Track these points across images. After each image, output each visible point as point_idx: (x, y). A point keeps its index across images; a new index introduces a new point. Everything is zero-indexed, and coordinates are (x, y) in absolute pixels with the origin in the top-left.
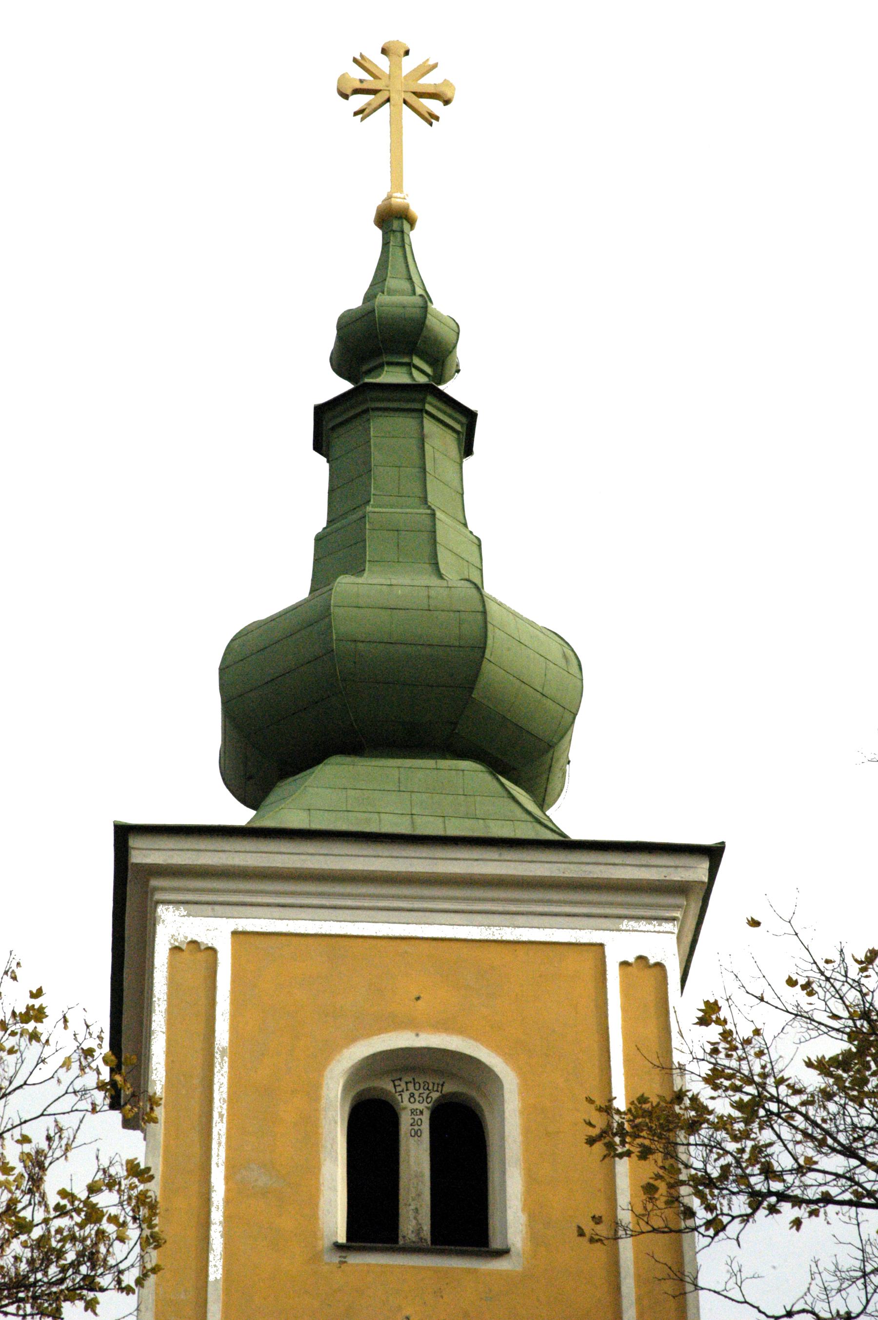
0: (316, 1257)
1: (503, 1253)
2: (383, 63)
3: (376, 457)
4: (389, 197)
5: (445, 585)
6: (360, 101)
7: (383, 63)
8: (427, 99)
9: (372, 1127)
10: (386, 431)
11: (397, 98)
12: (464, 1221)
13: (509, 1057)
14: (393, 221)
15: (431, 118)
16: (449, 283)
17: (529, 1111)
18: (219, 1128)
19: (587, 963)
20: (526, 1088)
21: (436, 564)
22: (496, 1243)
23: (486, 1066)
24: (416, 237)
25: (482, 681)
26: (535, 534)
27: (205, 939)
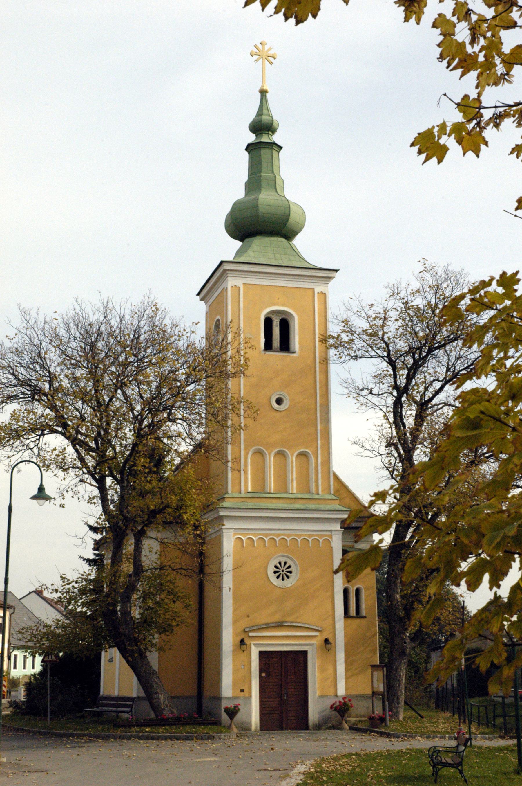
0: (260, 352)
1: (294, 352)
2: (260, 46)
3: (263, 159)
4: (262, 86)
5: (373, 444)
6: (256, 57)
7: (260, 46)
8: (270, 58)
9: (268, 322)
10: (265, 152)
11: (264, 58)
12: (285, 346)
13: (296, 312)
14: (263, 93)
15: (271, 63)
16: (277, 112)
17: (300, 324)
18: (318, 415)
19: (311, 292)
20: (299, 318)
21: (276, 189)
22: (292, 349)
23: (232, 208)
24: (268, 95)
25: (289, 223)
26: (297, 184)
27: (238, 285)
